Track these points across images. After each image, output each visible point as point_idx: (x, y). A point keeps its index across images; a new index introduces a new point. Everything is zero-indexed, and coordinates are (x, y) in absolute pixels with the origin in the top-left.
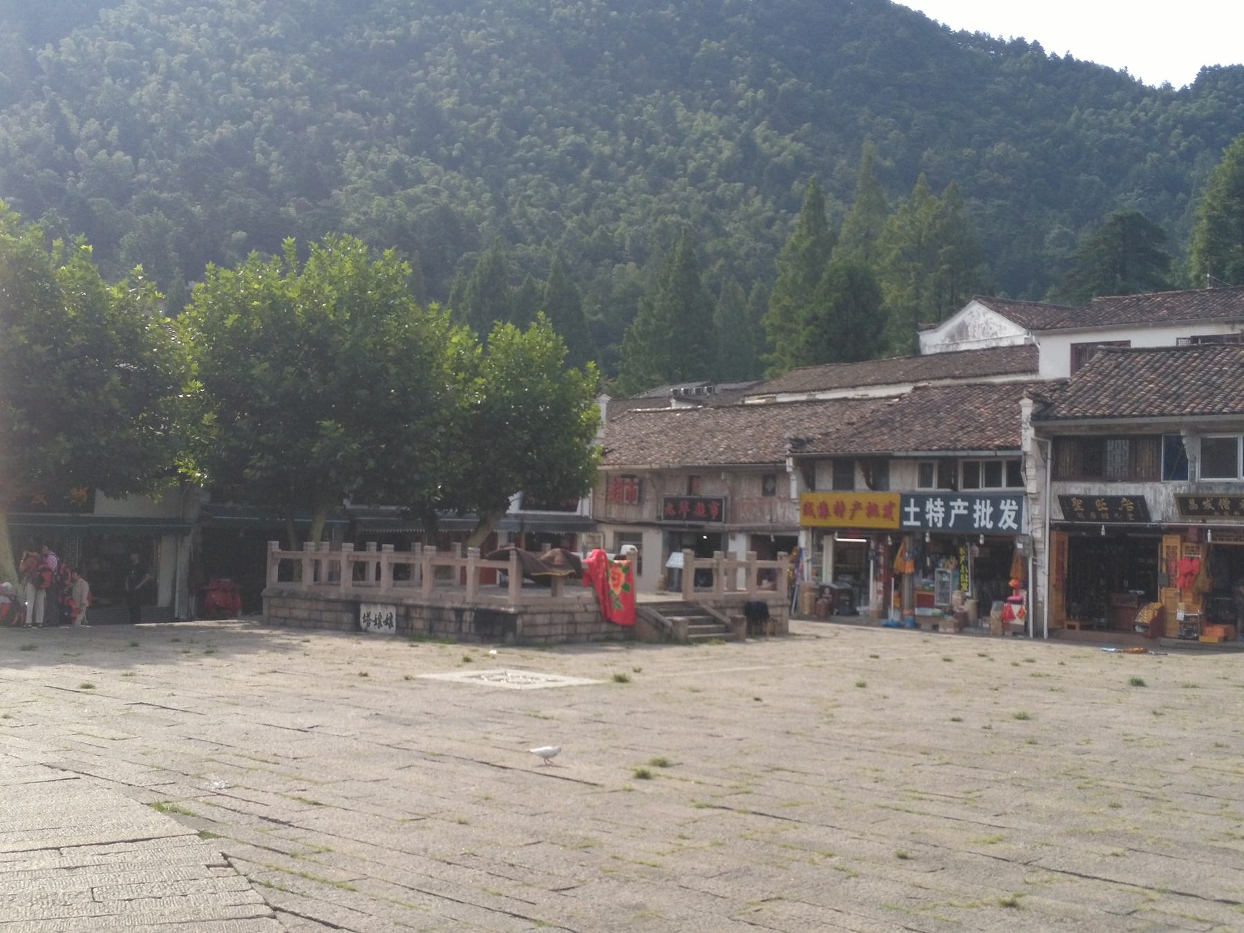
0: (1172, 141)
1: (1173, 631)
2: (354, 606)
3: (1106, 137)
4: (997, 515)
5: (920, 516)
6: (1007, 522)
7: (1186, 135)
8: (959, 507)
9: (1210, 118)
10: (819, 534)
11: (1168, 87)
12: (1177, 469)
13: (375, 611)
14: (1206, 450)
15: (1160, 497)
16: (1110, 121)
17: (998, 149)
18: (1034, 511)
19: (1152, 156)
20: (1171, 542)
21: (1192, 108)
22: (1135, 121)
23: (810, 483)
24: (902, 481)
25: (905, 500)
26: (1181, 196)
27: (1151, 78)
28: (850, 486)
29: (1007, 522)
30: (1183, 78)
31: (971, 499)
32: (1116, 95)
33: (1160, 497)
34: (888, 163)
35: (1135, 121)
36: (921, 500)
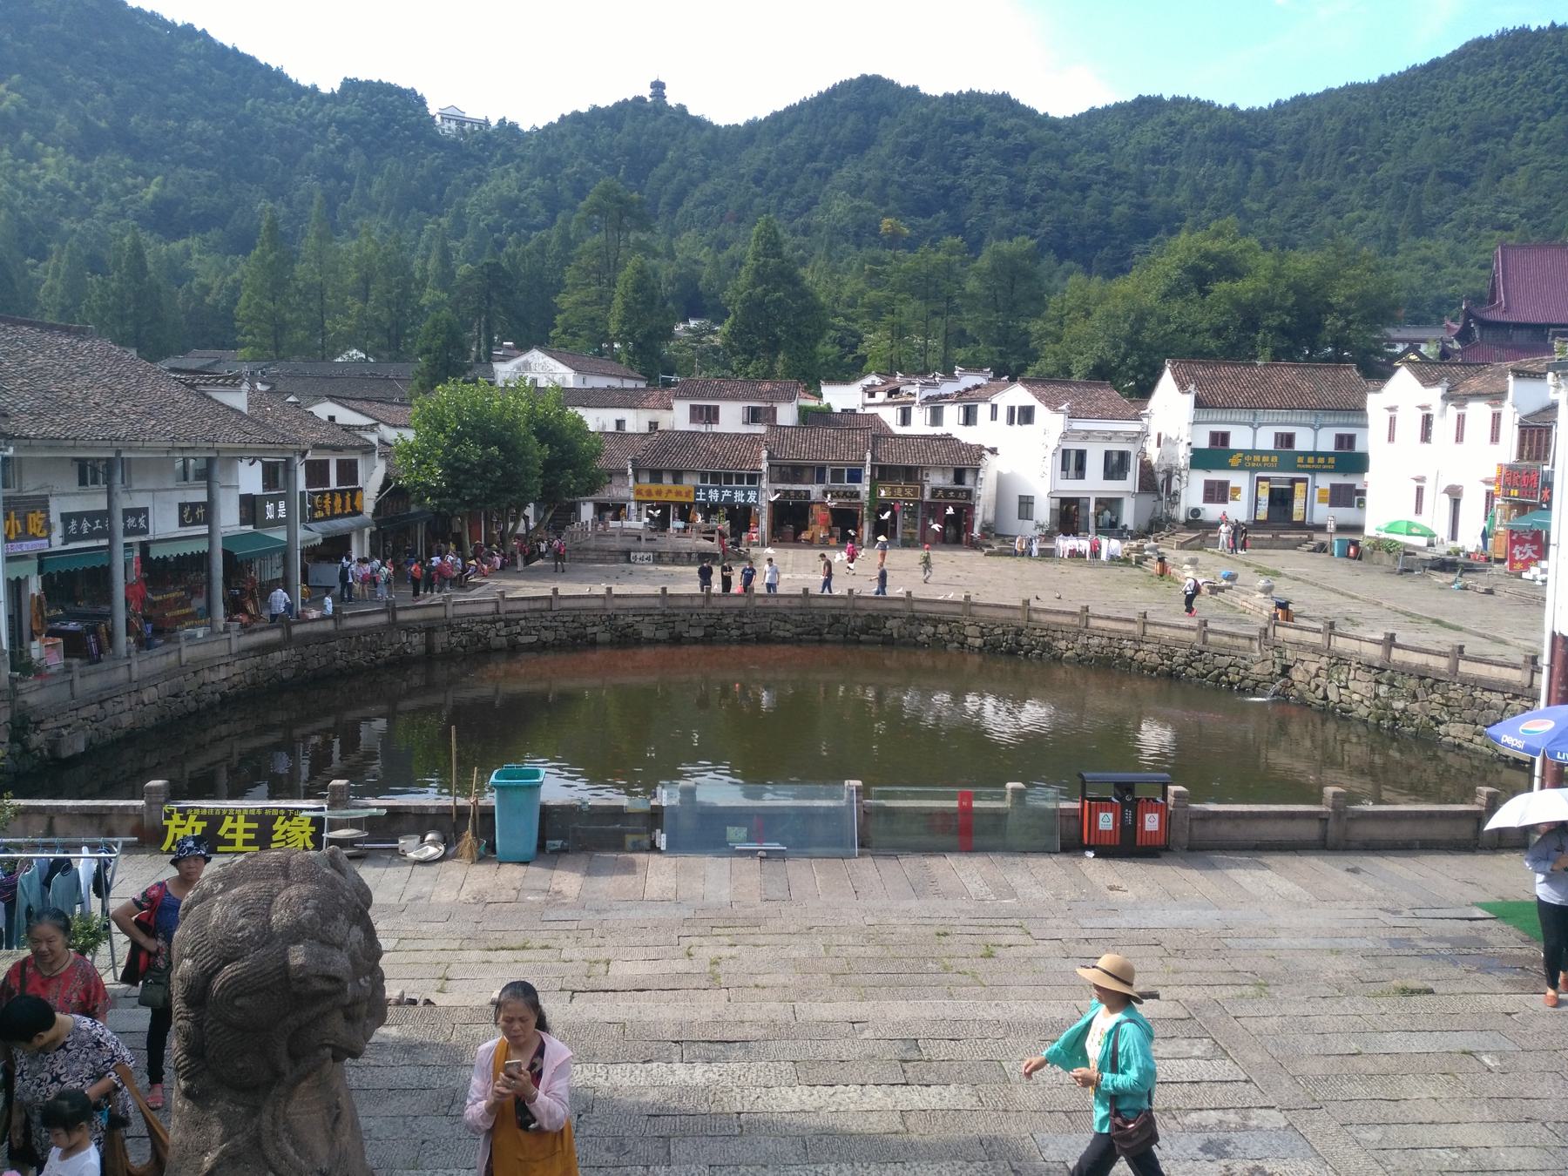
0: (330, 135)
1: (816, 541)
2: (627, 553)
3: (278, 125)
4: (746, 497)
5: (706, 496)
6: (752, 499)
7: (340, 132)
8: (727, 493)
9: (355, 122)
10: (640, 502)
11: (315, 88)
12: (821, 480)
13: (639, 555)
14: (833, 472)
15: (815, 490)
16: (280, 112)
17: (197, 125)
18: (766, 495)
19: (318, 149)
20: (816, 508)
21: (341, 112)
22: (299, 114)
23: (636, 479)
24: (690, 481)
25: (697, 489)
26: (344, 183)
27: (302, 75)
28: (660, 481)
29: (752, 499)
30: (329, 84)
31: (733, 490)
32: (279, 90)
33: (815, 490)
34: (103, 124)
35: (299, 114)
36: (706, 490)
